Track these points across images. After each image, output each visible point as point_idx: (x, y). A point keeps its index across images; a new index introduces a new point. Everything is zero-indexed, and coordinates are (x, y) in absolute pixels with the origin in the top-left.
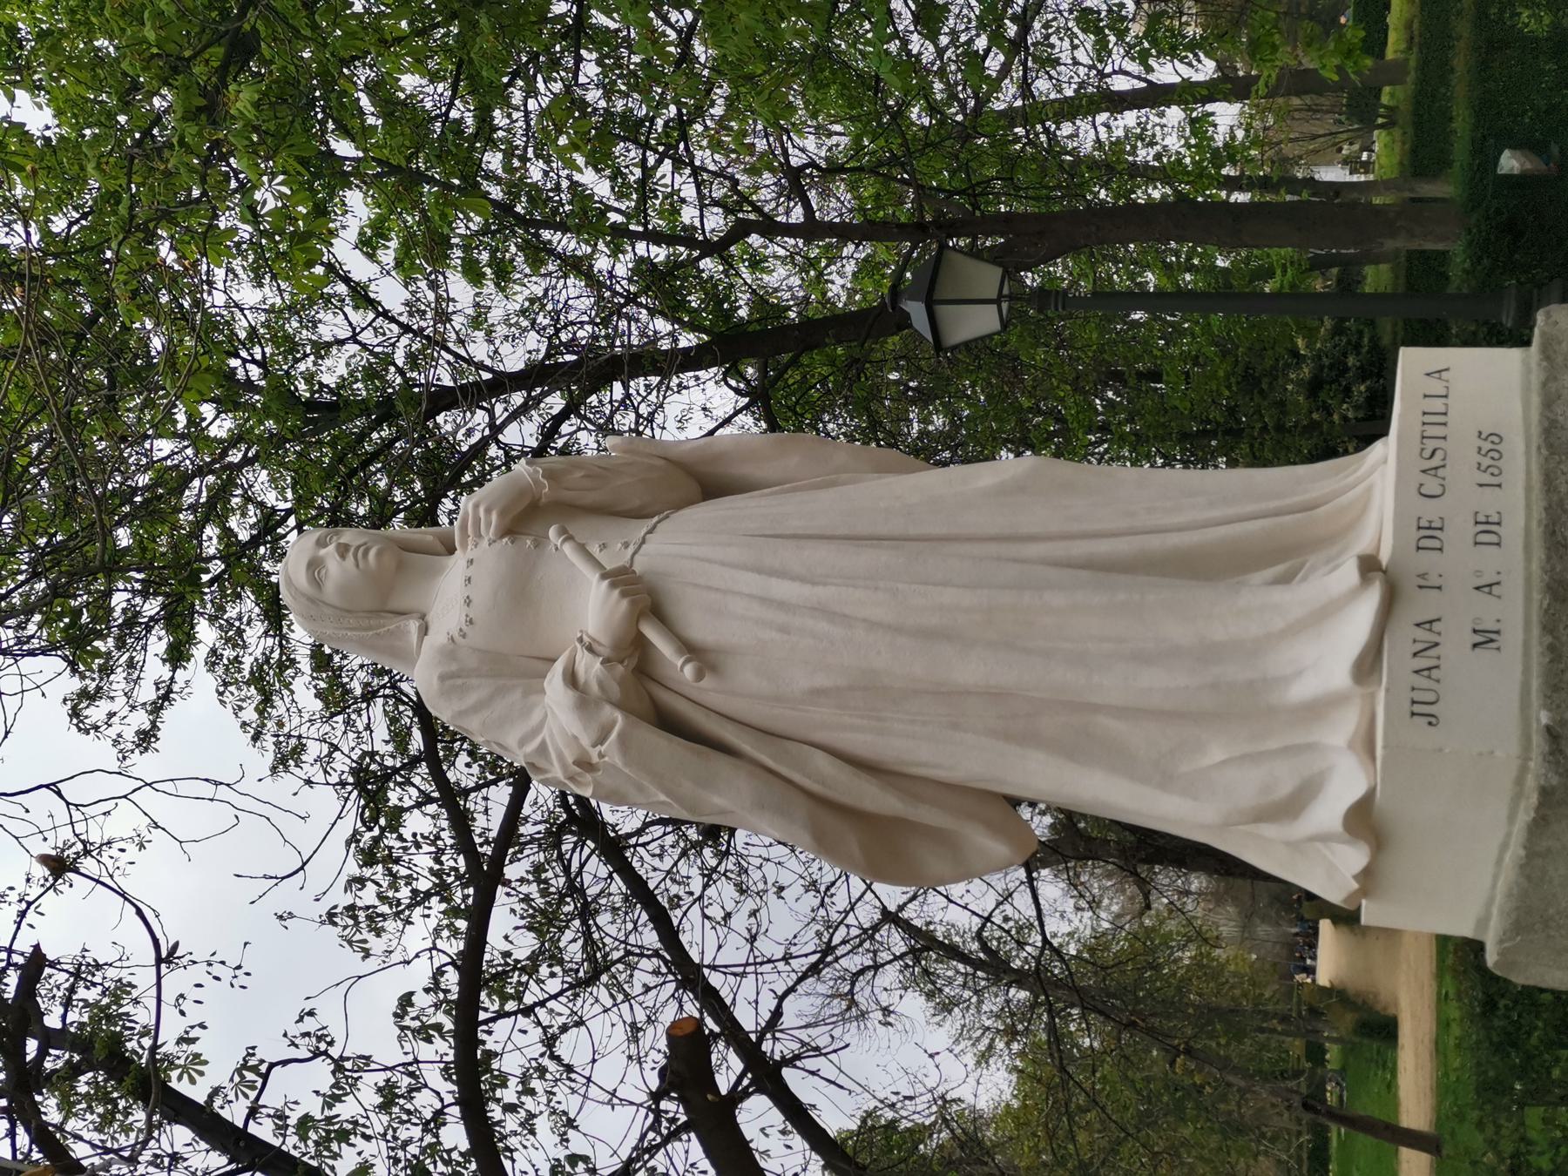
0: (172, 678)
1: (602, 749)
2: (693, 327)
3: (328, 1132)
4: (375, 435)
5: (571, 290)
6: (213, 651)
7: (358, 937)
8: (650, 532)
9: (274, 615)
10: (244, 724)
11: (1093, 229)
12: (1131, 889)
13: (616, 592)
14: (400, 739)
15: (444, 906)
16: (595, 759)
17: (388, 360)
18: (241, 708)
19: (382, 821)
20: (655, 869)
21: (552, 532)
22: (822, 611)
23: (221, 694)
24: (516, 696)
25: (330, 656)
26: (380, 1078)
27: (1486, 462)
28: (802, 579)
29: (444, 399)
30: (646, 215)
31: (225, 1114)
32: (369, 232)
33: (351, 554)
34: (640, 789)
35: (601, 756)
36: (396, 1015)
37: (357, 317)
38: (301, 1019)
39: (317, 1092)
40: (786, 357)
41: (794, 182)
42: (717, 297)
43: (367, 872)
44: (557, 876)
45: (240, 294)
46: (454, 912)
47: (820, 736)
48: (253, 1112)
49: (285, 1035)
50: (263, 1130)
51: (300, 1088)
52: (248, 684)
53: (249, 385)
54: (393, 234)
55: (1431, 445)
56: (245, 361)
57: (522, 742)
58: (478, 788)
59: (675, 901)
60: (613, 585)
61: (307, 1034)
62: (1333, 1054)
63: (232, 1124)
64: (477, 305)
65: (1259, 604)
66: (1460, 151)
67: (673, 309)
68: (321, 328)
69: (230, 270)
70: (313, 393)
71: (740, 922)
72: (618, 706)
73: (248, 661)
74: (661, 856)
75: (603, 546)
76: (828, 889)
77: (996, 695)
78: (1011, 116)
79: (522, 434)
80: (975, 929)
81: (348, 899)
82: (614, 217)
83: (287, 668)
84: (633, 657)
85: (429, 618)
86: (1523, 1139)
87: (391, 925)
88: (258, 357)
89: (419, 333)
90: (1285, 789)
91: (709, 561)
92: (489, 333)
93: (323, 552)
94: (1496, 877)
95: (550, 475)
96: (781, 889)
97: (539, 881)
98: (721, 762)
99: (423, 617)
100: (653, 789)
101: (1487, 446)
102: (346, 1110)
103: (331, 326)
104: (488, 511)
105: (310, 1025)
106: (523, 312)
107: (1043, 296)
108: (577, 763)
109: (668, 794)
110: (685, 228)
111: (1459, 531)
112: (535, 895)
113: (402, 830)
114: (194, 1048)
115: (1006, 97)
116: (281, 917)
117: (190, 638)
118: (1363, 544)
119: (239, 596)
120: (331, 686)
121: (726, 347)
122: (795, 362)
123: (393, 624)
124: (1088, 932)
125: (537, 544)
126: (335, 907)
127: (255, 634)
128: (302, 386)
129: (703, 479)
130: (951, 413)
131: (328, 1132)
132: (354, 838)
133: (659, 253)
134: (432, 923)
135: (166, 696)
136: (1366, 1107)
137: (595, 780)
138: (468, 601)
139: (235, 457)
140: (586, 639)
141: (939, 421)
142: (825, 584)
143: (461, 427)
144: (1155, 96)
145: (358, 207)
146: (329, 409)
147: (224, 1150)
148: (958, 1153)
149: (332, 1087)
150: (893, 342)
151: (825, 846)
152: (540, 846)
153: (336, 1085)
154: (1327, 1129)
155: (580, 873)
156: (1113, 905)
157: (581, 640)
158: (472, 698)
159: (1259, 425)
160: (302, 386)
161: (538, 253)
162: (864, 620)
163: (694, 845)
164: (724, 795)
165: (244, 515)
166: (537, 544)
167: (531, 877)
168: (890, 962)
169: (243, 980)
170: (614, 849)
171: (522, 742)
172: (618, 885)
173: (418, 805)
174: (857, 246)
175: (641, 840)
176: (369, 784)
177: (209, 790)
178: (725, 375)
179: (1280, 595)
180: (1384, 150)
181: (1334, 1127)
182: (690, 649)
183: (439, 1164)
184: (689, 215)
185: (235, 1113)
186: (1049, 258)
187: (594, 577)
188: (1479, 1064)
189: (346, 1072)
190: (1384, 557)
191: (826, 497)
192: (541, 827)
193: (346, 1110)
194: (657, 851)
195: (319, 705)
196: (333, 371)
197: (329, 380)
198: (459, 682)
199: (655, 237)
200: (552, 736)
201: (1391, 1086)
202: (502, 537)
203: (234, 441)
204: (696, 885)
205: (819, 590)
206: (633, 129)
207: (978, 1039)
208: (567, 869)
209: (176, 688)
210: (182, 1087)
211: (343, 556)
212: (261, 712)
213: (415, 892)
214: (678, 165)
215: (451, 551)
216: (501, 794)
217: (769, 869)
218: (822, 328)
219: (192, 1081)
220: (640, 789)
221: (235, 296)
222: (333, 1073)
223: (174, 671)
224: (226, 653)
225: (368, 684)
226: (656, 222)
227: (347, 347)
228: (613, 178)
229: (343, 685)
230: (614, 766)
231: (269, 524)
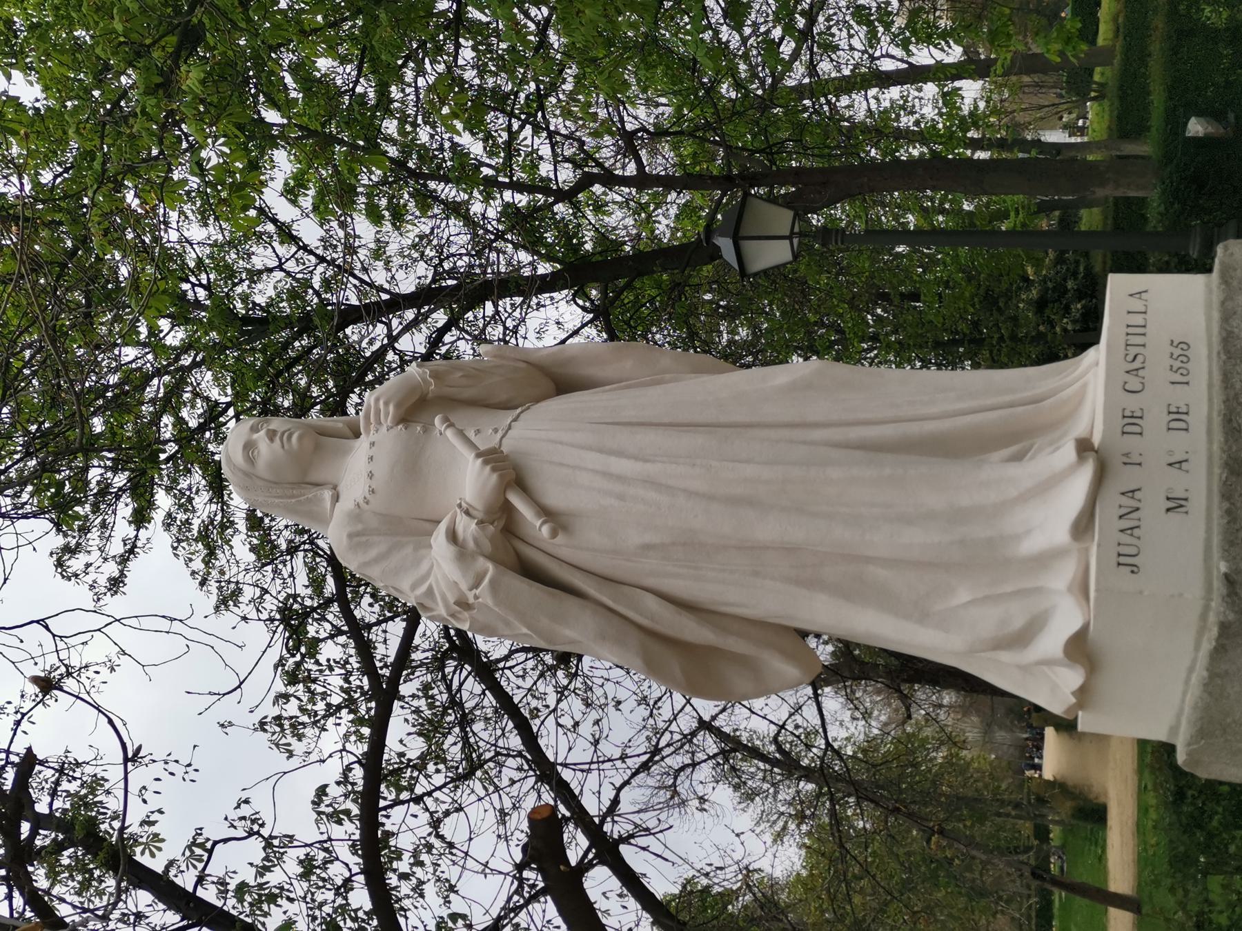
0: (136, 536)
1: (477, 592)
2: (549, 258)
3: (260, 895)
4: (297, 344)
6: (169, 515)
7: (283, 741)
8: (515, 420)
9: (217, 486)
10: (193, 573)
11: (866, 180)
12: (896, 703)
13: (488, 468)
14: (317, 584)
16: (471, 600)
17: (307, 284)
18: (191, 560)
19: (303, 650)
20: (519, 688)
21: (437, 420)
24: (409, 550)
25: (262, 519)
26: (301, 853)
28: (636, 458)
29: (351, 315)
30: (512, 169)
31: (178, 881)
32: (292, 183)
33: (277, 439)
34: (507, 624)
35: (476, 597)
36: (313, 803)
37: (282, 250)
38: (238, 806)
39: (251, 864)
40: (622, 282)
41: (629, 143)
42: (568, 235)
43: (291, 690)
44: (441, 693)
45: (190, 232)
46: (359, 721)
48: (200, 880)
49: (226, 819)
50: (209, 894)
51: (238, 861)
52: (196, 540)
53: (197, 304)
54: (311, 185)
56: (194, 285)
57: (414, 587)
58: (378, 623)
59: (535, 713)
60: (486, 462)
61: (244, 818)
62: (1055, 834)
63: (184, 889)
64: (378, 241)
65: (998, 476)
67: (533, 244)
68: (254, 259)
69: (182, 213)
71: (586, 729)
72: (490, 558)
73: (196, 523)
74: (523, 677)
75: (478, 432)
76: (656, 703)
77: (790, 550)
79: (413, 343)
80: (772, 735)
81: (276, 711)
82: (486, 171)
83: (228, 528)
84: (502, 520)
85: (340, 488)
86: (1206, 900)
87: (309, 732)
88: (204, 282)
89: (332, 263)
90: (1018, 623)
91: (561, 443)
92: (387, 262)
93: (255, 436)
94: (1184, 693)
95: (435, 375)
96: (619, 703)
97: (427, 697)
98: (571, 602)
99: (335, 488)
101: (1177, 352)
102: (274, 878)
103: (262, 257)
104: (386, 404)
105: (246, 810)
107: (826, 233)
108: (458, 603)
109: (529, 628)
111: (1155, 420)
112: (424, 708)
113: (318, 657)
114: (154, 829)
115: (797, 75)
116: (222, 726)
117: (151, 505)
118: (1079, 430)
119: (189, 471)
120: (262, 542)
121: (575, 274)
122: (628, 286)
123: (311, 493)
124: (862, 737)
125: (425, 430)
126: (266, 717)
127: (202, 501)
128: (239, 305)
129: (557, 379)
130: (754, 327)
131: (260, 895)
132: (281, 663)
133: (522, 200)
134: (342, 730)
136: (1082, 875)
137: (472, 618)
138: (371, 475)
139: (186, 361)
140: (464, 505)
141: (743, 333)
142: (653, 462)
143: (365, 337)
144: (914, 75)
145: (283, 164)
146: (261, 323)
147: (178, 910)
149: (263, 860)
150: (707, 270)
151: (653, 669)
152: (428, 669)
153: (267, 859)
154: (1051, 893)
155: (459, 690)
156: (882, 716)
157: (460, 506)
158: (373, 553)
159: (996, 336)
160: (239, 305)
161: (426, 199)
162: (684, 490)
163: (550, 668)
164: (573, 629)
166: (425, 430)
167: (420, 694)
168: (705, 761)
169: (192, 775)
170: (486, 672)
171: (414, 587)
172: (490, 700)
173: (332, 637)
174: (679, 194)
175: (508, 664)
176: (292, 620)
177: (165, 625)
178: (574, 296)
179: (1014, 470)
180: (1096, 116)
182: (547, 513)
183: (348, 920)
184: (545, 169)
185: (186, 880)
186: (831, 203)
187: (470, 456)
188: (1171, 841)
189: (274, 848)
190: (1096, 440)
191: (654, 392)
192: (429, 654)
193: (274, 878)
194: (521, 673)
195: (252, 557)
196: (264, 292)
197: (261, 300)
198: (364, 539)
199: (518, 187)
200: (437, 581)
201: (1102, 859)
202: (397, 424)
203: (185, 348)
204: (552, 700)
205: (648, 466)
206: (501, 101)
207: (775, 822)
208: (449, 688)
209: (139, 544)
210: (145, 860)
211: (272, 440)
213: (329, 705)
215: (357, 435)
216: (397, 628)
217: (609, 687)
218: (651, 258)
219: (153, 855)
221: (186, 234)
223: (138, 530)
224: (179, 516)
225: (291, 541)
227: (275, 273)
228: (485, 140)
229: (272, 542)
230: (487, 606)
231: (213, 414)
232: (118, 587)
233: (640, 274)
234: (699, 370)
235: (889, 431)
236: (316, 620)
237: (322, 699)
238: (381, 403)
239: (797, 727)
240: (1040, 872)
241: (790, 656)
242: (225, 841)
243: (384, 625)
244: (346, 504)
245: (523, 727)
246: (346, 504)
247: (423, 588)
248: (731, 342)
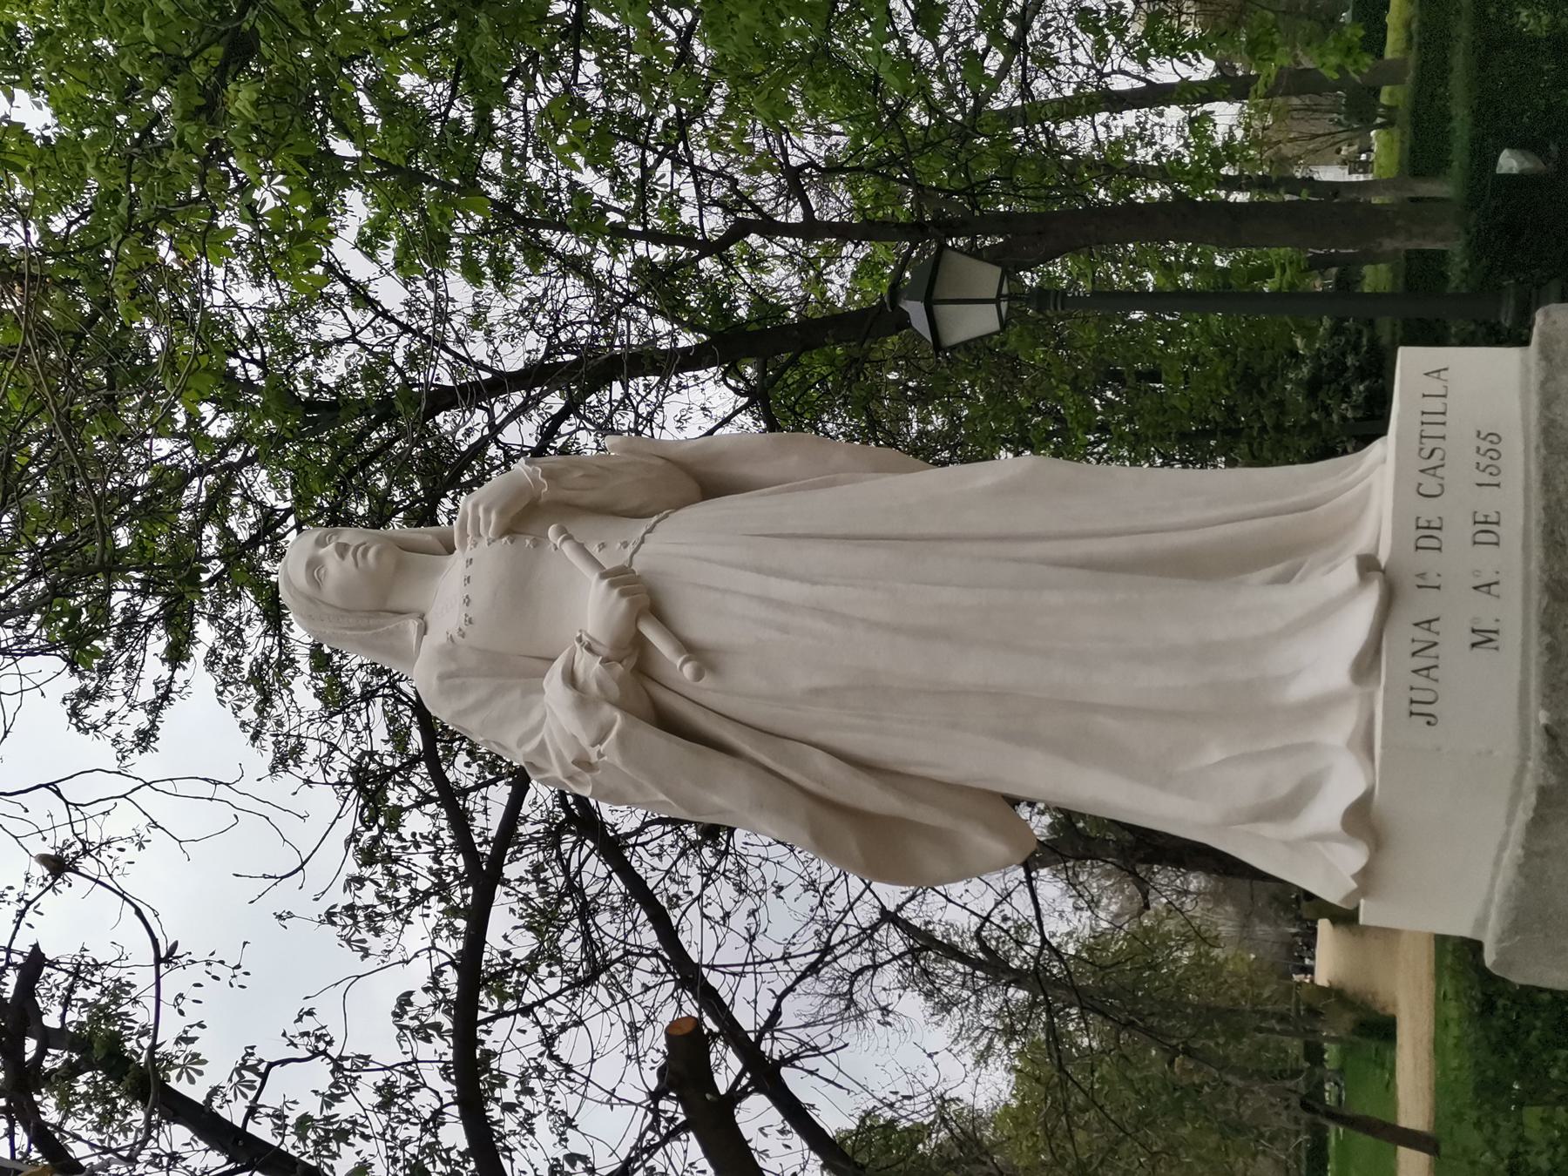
0: (171, 678)
1: (602, 748)
2: (693, 327)
4: (374, 435)
5: (570, 289)
6: (213, 651)
7: (357, 936)
8: (649, 531)
9: (274, 615)
10: (243, 724)
12: (1130, 889)
13: (616, 592)
14: (399, 738)
15: (443, 905)
16: (594, 759)
17: (387, 360)
18: (240, 708)
19: (382, 821)
20: (654, 869)
22: (820, 610)
23: (220, 693)
24: (516, 695)
25: (329, 656)
27: (1485, 461)
28: (801, 579)
29: (443, 399)
30: (645, 215)
31: (224, 1113)
32: (368, 232)
34: (639, 788)
35: (600, 755)
36: (394, 1014)
37: (356, 317)
38: (300, 1019)
39: (316, 1092)
40: (785, 357)
41: (793, 182)
42: (717, 298)
43: (367, 872)
44: (556, 876)
45: (239, 294)
46: (453, 912)
47: (819, 736)
48: (252, 1112)
49: (284, 1035)
50: (262, 1130)
51: (299, 1088)
52: (247, 683)
53: (249, 385)
55: (1429, 444)
56: (244, 361)
58: (477, 788)
59: (674, 901)
60: (612, 585)
61: (306, 1034)
62: (1331, 1053)
64: (476, 305)
65: (1258, 603)
66: (1459, 156)
67: (672, 308)
69: (229, 270)
70: (312, 392)
71: (739, 921)
72: (617, 705)
73: (247, 661)
74: (660, 856)
75: (603, 546)
76: (827, 888)
78: (1009, 116)
79: (521, 434)
80: (973, 929)
81: (347, 899)
83: (287, 667)
84: (633, 657)
85: (428, 617)
86: (1521, 1138)
87: (389, 925)
88: (258, 357)
90: (1283, 788)
91: (709, 561)
92: (488, 333)
93: (322, 551)
95: (549, 475)
96: (780, 888)
97: (538, 881)
99: (422, 617)
100: (652, 789)
101: (1485, 445)
102: (345, 1110)
103: (331, 325)
104: (487, 511)
105: (309, 1024)
106: (522, 312)
107: (1044, 296)
110: (684, 227)
111: (1458, 531)
112: (534, 895)
113: (401, 830)
115: (1006, 97)
116: (280, 917)
117: (190, 638)
118: (1362, 544)
119: (239, 596)
120: (330, 686)
121: (725, 346)
122: (793, 363)
123: (393, 623)
125: (536, 543)
128: (301, 386)
129: (703, 479)
130: (951, 413)
132: (354, 837)
133: (659, 253)
134: (431, 923)
135: (165, 695)
139: (235, 456)
140: (585, 638)
141: (938, 421)
143: (461, 426)
145: (357, 208)
146: (329, 409)
147: (223, 1150)
148: (957, 1153)
150: (892, 342)
151: (823, 845)
152: (539, 845)
153: (335, 1085)
154: (1326, 1129)
155: (579, 872)
156: (1112, 905)
157: (580, 640)
158: (470, 699)
159: (1257, 426)
160: (301, 386)
161: (537, 253)
162: (863, 620)
163: (693, 845)
165: (243, 515)
166: (536, 543)
167: (530, 877)
168: (888, 962)
169: (242, 979)
170: (613, 849)
172: (617, 884)
173: (418, 805)
174: (856, 246)
176: (368, 783)
177: (208, 789)
178: (724, 374)
179: (1279, 594)
181: (1332, 1127)
182: (689, 649)
183: (438, 1163)
184: (688, 214)
185: (234, 1113)
186: (1048, 258)
187: (593, 576)
189: (345, 1072)
190: (1383, 558)
192: (541, 827)
193: (345, 1110)
194: (657, 851)
195: (318, 704)
196: (333, 370)
197: (328, 379)
198: (458, 681)
199: (654, 237)
200: (551, 734)
201: (1390, 1086)
202: (501, 536)
203: (234, 440)
204: (695, 884)
205: (818, 589)
206: (633, 129)
207: (977, 1039)
208: (566, 869)
209: (175, 688)
211: (342, 556)
212: (260, 711)
213: (414, 891)
214: (677, 165)
215: (450, 550)
216: (500, 794)
218: (822, 328)
219: (192, 1081)
220: (639, 788)
221: (235, 296)
222: (332, 1072)
223: (173, 671)
224: (225, 653)
225: (367, 684)
226: (656, 222)
227: (346, 346)
228: (612, 178)
229: (342, 685)
231: (269, 524)
232: (149, 743)
233: (807, 348)
234: (881, 469)
235: (1122, 546)
236: (398, 784)
237: (406, 884)
238: (481, 509)
239: (1005, 919)
240: (1311, 1102)
241: (992, 828)
242: (283, 1062)
243: (483, 790)
244: (437, 637)
245: (660, 920)
246: (437, 637)
247: (535, 743)
248: (922, 433)
